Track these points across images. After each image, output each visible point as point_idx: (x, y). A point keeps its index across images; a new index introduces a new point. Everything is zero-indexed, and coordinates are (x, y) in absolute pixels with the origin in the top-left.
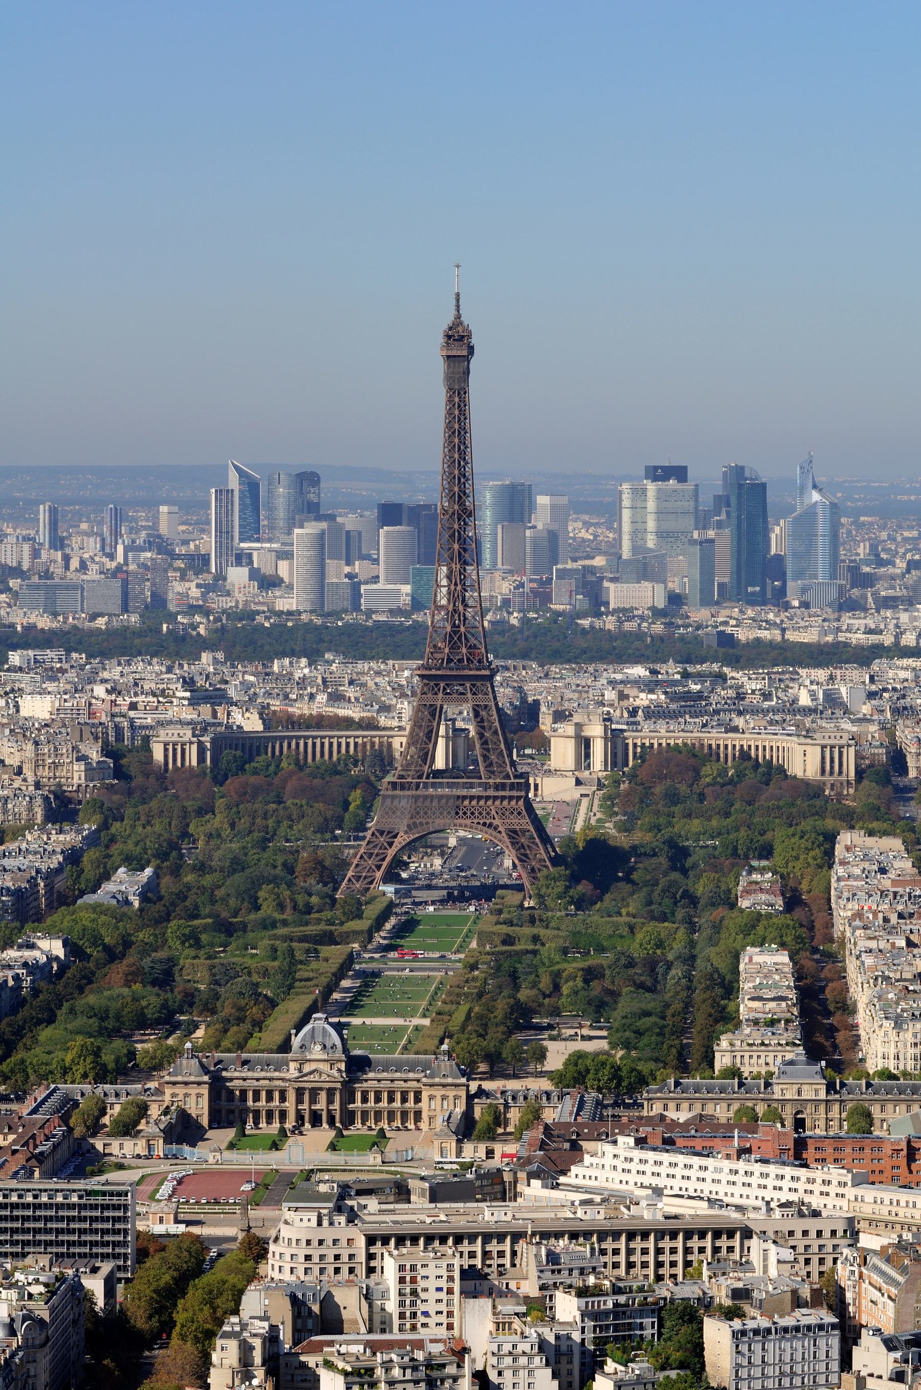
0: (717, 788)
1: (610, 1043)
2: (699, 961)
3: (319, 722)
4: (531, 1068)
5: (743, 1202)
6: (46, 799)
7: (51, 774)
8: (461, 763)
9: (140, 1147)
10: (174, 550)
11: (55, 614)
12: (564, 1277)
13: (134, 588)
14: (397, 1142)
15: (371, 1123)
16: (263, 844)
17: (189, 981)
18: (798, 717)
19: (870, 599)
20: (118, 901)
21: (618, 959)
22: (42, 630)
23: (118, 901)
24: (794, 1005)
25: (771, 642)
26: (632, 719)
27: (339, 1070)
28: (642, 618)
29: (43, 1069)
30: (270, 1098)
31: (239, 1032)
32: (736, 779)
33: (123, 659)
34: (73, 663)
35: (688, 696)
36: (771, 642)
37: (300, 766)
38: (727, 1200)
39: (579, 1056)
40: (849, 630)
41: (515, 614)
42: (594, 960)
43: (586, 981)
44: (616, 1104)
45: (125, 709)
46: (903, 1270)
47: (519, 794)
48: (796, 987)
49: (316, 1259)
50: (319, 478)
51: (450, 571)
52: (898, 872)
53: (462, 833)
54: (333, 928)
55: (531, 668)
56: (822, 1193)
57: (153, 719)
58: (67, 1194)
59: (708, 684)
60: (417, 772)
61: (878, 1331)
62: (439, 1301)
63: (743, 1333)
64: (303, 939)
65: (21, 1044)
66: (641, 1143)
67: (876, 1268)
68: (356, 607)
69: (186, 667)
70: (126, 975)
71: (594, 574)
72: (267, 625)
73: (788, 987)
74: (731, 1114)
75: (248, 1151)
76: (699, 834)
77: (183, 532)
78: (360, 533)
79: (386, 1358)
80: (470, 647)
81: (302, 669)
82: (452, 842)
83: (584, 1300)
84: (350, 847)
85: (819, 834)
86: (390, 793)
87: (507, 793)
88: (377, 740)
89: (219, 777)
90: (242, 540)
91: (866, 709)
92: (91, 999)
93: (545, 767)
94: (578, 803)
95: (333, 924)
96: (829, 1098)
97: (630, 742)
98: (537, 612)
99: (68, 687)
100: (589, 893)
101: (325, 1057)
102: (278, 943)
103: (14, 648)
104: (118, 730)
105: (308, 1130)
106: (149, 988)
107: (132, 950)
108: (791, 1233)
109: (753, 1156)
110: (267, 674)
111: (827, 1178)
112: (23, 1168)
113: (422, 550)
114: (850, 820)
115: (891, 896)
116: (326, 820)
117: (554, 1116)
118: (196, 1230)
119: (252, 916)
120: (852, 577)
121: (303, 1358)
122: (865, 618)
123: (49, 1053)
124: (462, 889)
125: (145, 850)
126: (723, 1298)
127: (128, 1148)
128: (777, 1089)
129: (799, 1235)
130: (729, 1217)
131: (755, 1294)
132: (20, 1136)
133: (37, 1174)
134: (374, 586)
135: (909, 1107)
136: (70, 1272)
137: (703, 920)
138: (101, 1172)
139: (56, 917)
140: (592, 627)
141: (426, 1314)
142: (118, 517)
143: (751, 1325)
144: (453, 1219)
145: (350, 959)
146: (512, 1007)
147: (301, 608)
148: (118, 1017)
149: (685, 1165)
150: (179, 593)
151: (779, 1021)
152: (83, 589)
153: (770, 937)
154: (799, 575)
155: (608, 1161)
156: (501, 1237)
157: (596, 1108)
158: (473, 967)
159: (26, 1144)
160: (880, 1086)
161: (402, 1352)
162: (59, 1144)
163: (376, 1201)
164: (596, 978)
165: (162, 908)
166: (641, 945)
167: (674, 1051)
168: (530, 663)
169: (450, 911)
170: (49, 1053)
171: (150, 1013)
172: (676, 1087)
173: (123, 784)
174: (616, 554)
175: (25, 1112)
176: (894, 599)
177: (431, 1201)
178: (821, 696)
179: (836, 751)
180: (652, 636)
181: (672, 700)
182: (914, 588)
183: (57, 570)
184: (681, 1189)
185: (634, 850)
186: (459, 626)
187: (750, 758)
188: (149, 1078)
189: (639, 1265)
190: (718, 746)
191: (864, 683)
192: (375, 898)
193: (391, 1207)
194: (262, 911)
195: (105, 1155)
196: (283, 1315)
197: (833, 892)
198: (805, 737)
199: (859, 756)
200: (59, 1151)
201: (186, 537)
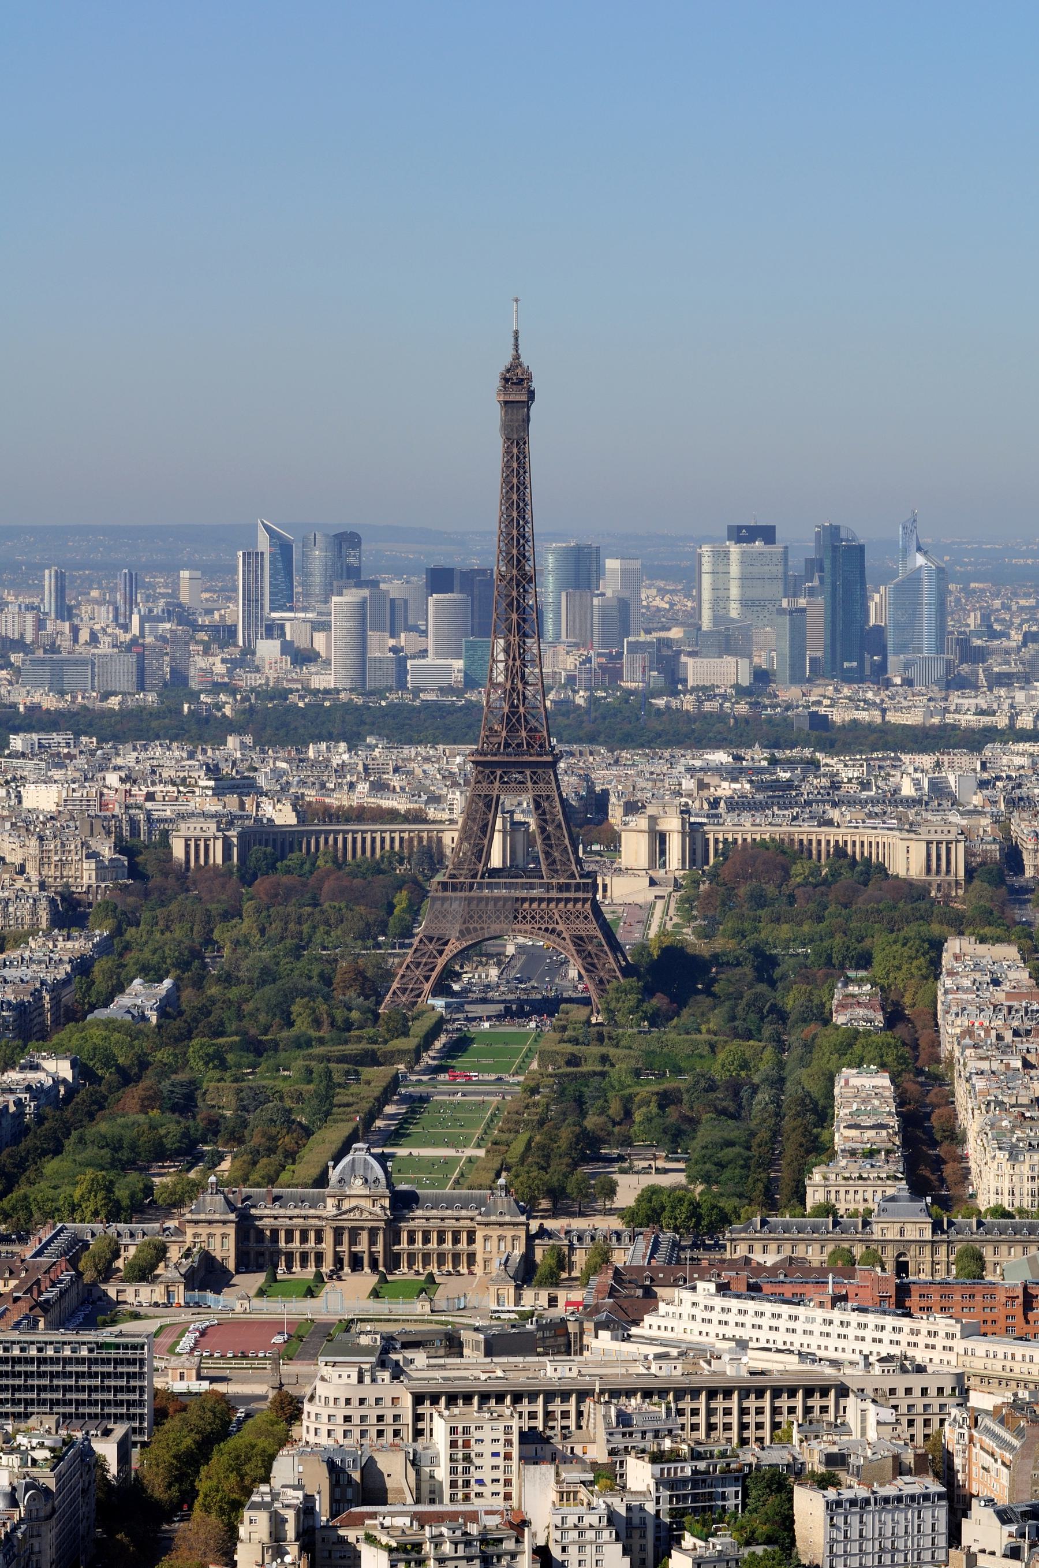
0: (809, 888)
1: (688, 1177)
2: (788, 1084)
3: (360, 814)
4: (599, 1204)
5: (838, 1356)
6: (52, 901)
7: (58, 874)
8: (520, 861)
9: (158, 1293)
10: (196, 621)
11: (62, 693)
12: (636, 1441)
13: (151, 663)
14: (448, 1288)
15: (418, 1266)
16: (297, 952)
17: (213, 1106)
18: (901, 809)
19: (982, 676)
20: (133, 1017)
21: (698, 1082)
22: (48, 710)
23: (133, 1017)
24: (896, 1134)
25: (870, 724)
26: (713, 812)
27: (383, 1207)
28: (725, 697)
29: (49, 1206)
30: (304, 1239)
31: (270, 1164)
32: (830, 879)
33: (138, 744)
34: (82, 748)
35: (776, 785)
36: (870, 724)
37: (339, 864)
38: (821, 1353)
39: (653, 1191)
40: (957, 711)
41: (581, 693)
42: (670, 1083)
43: (662, 1107)
44: (695, 1246)
45: (140, 800)
46: (1019, 1433)
47: (585, 895)
48: (898, 1114)
49: (356, 1420)
50: (360, 539)
51: (508, 644)
52: (1013, 984)
53: (521, 940)
54: (375, 1047)
55: (600, 754)
56: (927, 1346)
57: (172, 811)
58: (76, 1346)
59: (798, 771)
60: (470, 870)
61: (990, 1502)
62: (495, 1467)
63: (839, 1503)
64: (342, 1059)
65: (23, 1178)
66: (723, 1289)
67: (988, 1431)
68: (402, 685)
69: (210, 752)
70: (143, 1100)
71: (670, 647)
72: (301, 705)
73: (889, 1113)
74: (825, 1257)
75: (279, 1299)
76: (789, 940)
77: (207, 600)
78: (406, 601)
79: (435, 1531)
80: (531, 730)
81: (341, 754)
82: (510, 950)
83: (659, 1467)
84: (395, 955)
85: (924, 941)
86: (440, 894)
87: (571, 895)
88: (425, 835)
89: (248, 877)
90: (273, 609)
91: (977, 800)
92: (103, 1127)
93: (615, 866)
94: (652, 906)
95: (375, 1042)
96: (936, 1238)
97: (711, 836)
98: (605, 691)
99: (77, 775)
100: (665, 1007)
101: (367, 1192)
102: (313, 1063)
103: (16, 731)
104: (133, 823)
105: (347, 1275)
106: (168, 1114)
107: (149, 1072)
108: (892, 1391)
109: (849, 1304)
110: (301, 761)
111: (932, 1328)
112: (26, 1317)
113: (476, 620)
114: (959, 925)
115: (1005, 1011)
116: (367, 924)
117: (625, 1259)
118: (221, 1388)
119: (285, 1034)
120: (961, 651)
121: (342, 1532)
122: (976, 697)
123: (55, 1188)
124: (521, 1003)
125: (164, 959)
126: (815, 1464)
127: (144, 1295)
128: (876, 1228)
129: (901, 1393)
130: (822, 1373)
131: (852, 1460)
132: (23, 1282)
133: (41, 1325)
134: (422, 662)
135: (1025, 1248)
136: (79, 1435)
137: (793, 1038)
138: (114, 1322)
139: (63, 1034)
140: (668, 707)
141: (480, 1482)
142: (133, 583)
143: (847, 1494)
144: (511, 1375)
145: (395, 1082)
146: (577, 1136)
147: (340, 686)
148: (133, 1148)
149: (773, 1315)
150: (201, 669)
151: (879, 1151)
152: (93, 664)
153: (868, 1057)
154: (901, 649)
155: (686, 1309)
156: (565, 1396)
157: (672, 1250)
158: (534, 1091)
159: (29, 1290)
160: (993, 1225)
161: (454, 1525)
162: (66, 1291)
163: (425, 1355)
164: (673, 1103)
165: (183, 1025)
166: (723, 1066)
167: (760, 1185)
168: (598, 748)
169: (508, 1028)
170: (55, 1188)
171: (169, 1143)
172: (762, 1226)
173: (139, 884)
174: (695, 625)
175: (28, 1255)
176: (1009, 675)
177: (487, 1355)
178: (926, 786)
179: (944, 847)
180: (735, 718)
181: (758, 789)
182: (1031, 664)
183: (65, 642)
184: (768, 1341)
185: (715, 959)
186: (517, 707)
187: (846, 855)
188: (168, 1216)
189: (720, 1427)
190: (810, 841)
191: (974, 770)
192: (423, 1013)
193: (441, 1361)
194: (295, 1028)
195: (119, 1303)
196: (320, 1484)
197: (939, 1007)
198: (908, 831)
199: (969, 853)
200: (67, 1298)
201: (209, 605)
